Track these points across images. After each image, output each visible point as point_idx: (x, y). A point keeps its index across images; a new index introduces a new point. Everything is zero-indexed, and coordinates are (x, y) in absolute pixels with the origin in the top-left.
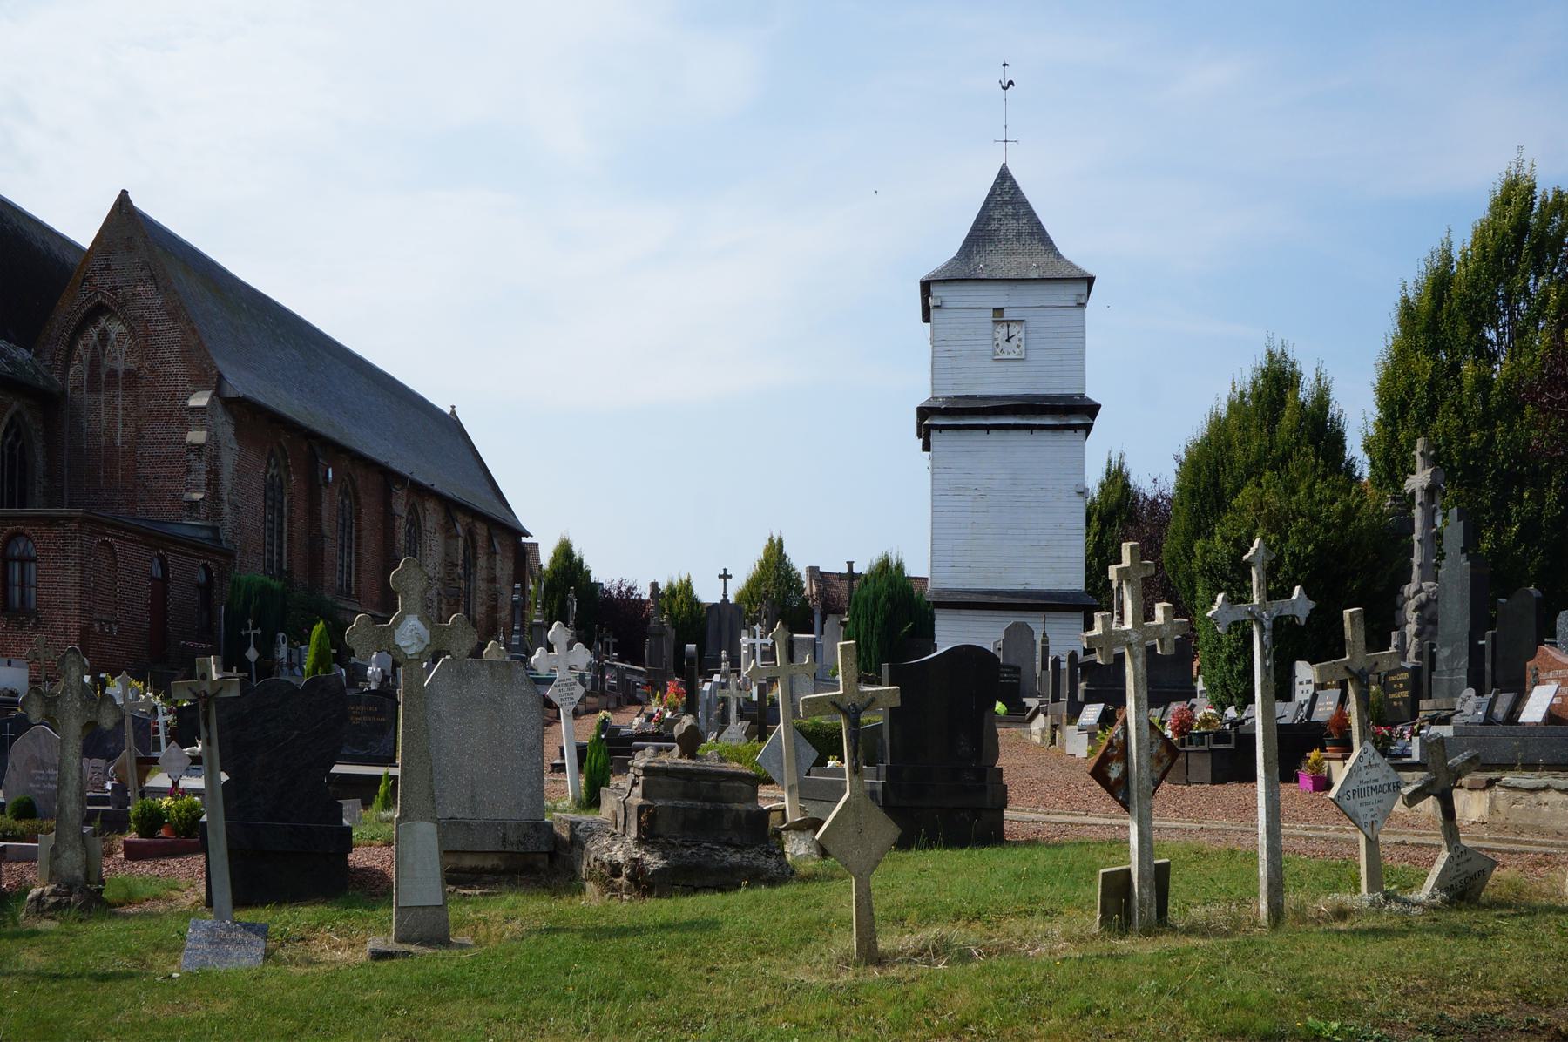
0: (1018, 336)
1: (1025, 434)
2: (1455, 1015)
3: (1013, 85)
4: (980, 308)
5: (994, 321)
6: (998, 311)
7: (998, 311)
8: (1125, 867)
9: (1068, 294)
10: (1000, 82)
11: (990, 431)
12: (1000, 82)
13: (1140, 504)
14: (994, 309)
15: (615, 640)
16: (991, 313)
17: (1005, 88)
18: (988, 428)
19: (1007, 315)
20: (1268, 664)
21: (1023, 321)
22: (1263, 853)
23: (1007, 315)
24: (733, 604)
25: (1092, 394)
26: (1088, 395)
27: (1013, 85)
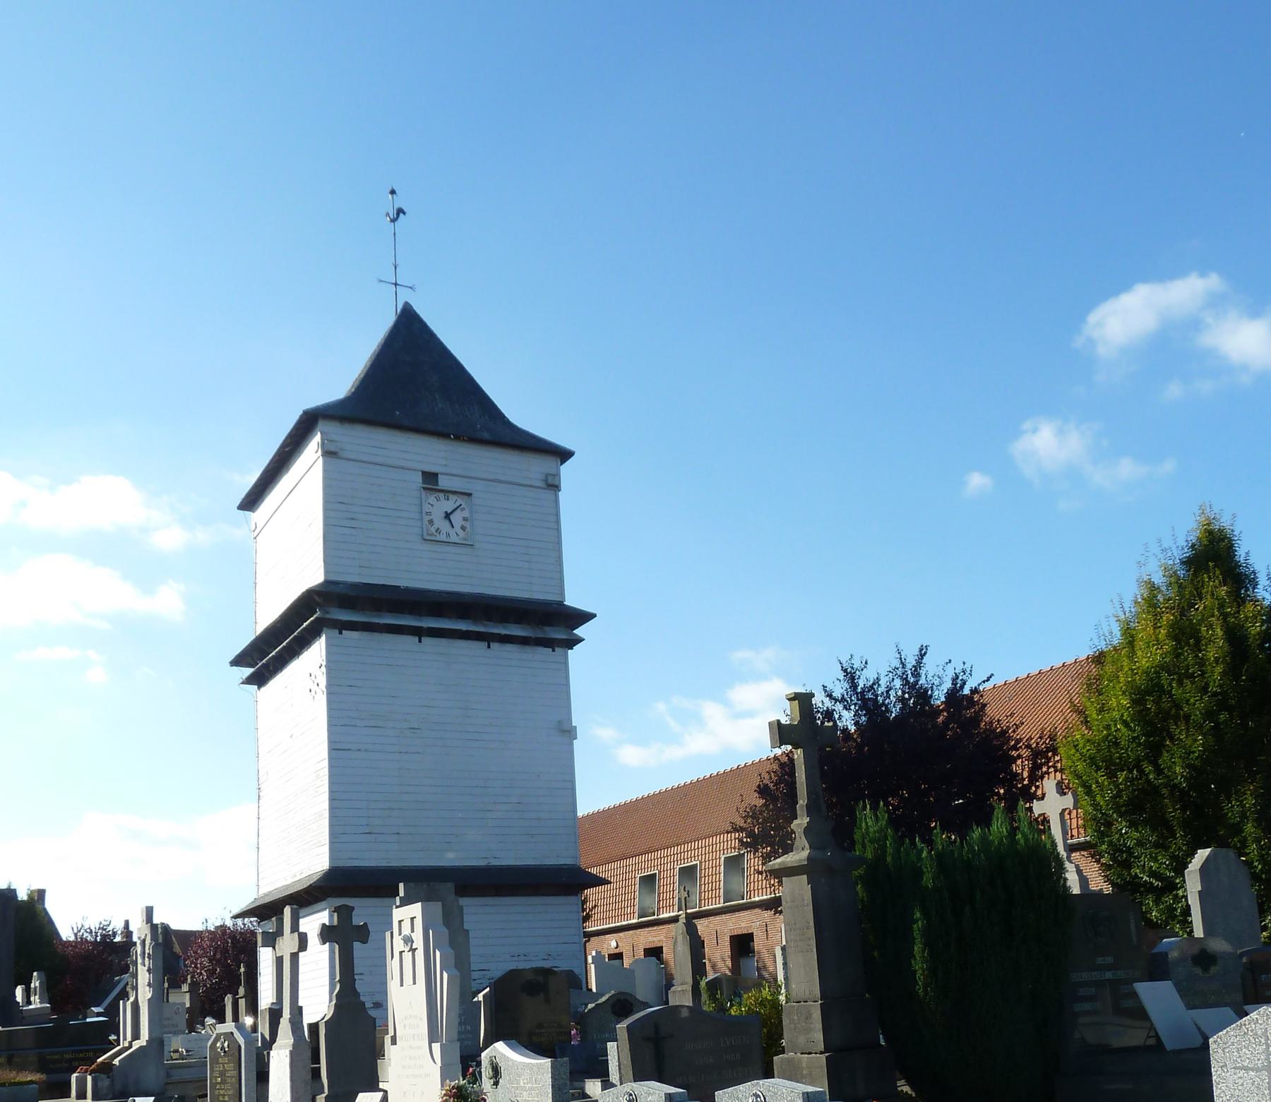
0: (452, 532)
1: (477, 647)
2: (235, 1035)
3: (404, 213)
4: (402, 468)
5: (423, 488)
6: (430, 478)
7: (430, 478)
8: (775, 1072)
9: (535, 466)
11: (423, 639)
13: (237, 997)
14: (424, 473)
15: (448, 1081)
16: (418, 478)
17: (393, 221)
18: (419, 633)
20: (934, 824)
21: (469, 495)
22: (263, 1028)
23: (443, 482)
24: (22, 901)
25: (574, 599)
26: (569, 602)
27: (404, 213)
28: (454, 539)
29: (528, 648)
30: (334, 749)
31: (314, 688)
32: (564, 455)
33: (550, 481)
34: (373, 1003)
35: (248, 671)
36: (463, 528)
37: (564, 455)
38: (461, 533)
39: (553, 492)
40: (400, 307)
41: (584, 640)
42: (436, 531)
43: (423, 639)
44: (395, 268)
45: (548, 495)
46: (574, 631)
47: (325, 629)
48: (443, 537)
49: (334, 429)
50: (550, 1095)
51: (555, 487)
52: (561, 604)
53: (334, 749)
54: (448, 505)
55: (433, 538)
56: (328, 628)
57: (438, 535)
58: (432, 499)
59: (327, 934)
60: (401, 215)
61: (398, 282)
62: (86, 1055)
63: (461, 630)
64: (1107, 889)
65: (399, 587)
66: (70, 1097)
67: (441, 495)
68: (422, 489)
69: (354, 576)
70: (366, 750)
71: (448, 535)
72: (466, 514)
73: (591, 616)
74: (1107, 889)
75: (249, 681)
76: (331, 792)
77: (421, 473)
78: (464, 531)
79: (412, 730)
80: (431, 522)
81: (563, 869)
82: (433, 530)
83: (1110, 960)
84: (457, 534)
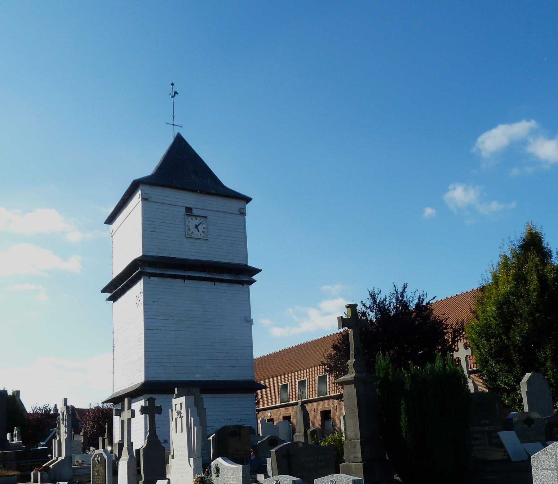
1: (209, 284)
6: (189, 210)
7: (189, 210)
9: (235, 205)
16: (184, 210)
21: (206, 217)
23: (195, 212)
25: (252, 263)
28: (199, 237)
29: (232, 285)
30: (147, 329)
31: (138, 302)
32: (248, 200)
33: (242, 211)
35: (109, 295)
36: (203, 232)
37: (248, 200)
38: (203, 234)
39: (243, 216)
41: (256, 281)
42: (192, 233)
44: (174, 118)
45: (240, 217)
46: (252, 277)
47: (143, 276)
48: (194, 236)
49: (147, 188)
50: (242, 481)
51: (244, 214)
53: (147, 329)
54: (197, 222)
55: (190, 236)
56: (144, 276)
57: (192, 235)
58: (190, 219)
61: (175, 124)
63: (202, 277)
64: (486, 390)
65: (175, 258)
67: (194, 218)
68: (185, 215)
69: (155, 253)
70: (161, 330)
71: (197, 235)
72: (205, 226)
74: (486, 390)
75: (109, 299)
76: (145, 348)
77: (185, 208)
78: (204, 233)
79: (181, 321)
80: (189, 229)
82: (190, 233)
84: (200, 234)
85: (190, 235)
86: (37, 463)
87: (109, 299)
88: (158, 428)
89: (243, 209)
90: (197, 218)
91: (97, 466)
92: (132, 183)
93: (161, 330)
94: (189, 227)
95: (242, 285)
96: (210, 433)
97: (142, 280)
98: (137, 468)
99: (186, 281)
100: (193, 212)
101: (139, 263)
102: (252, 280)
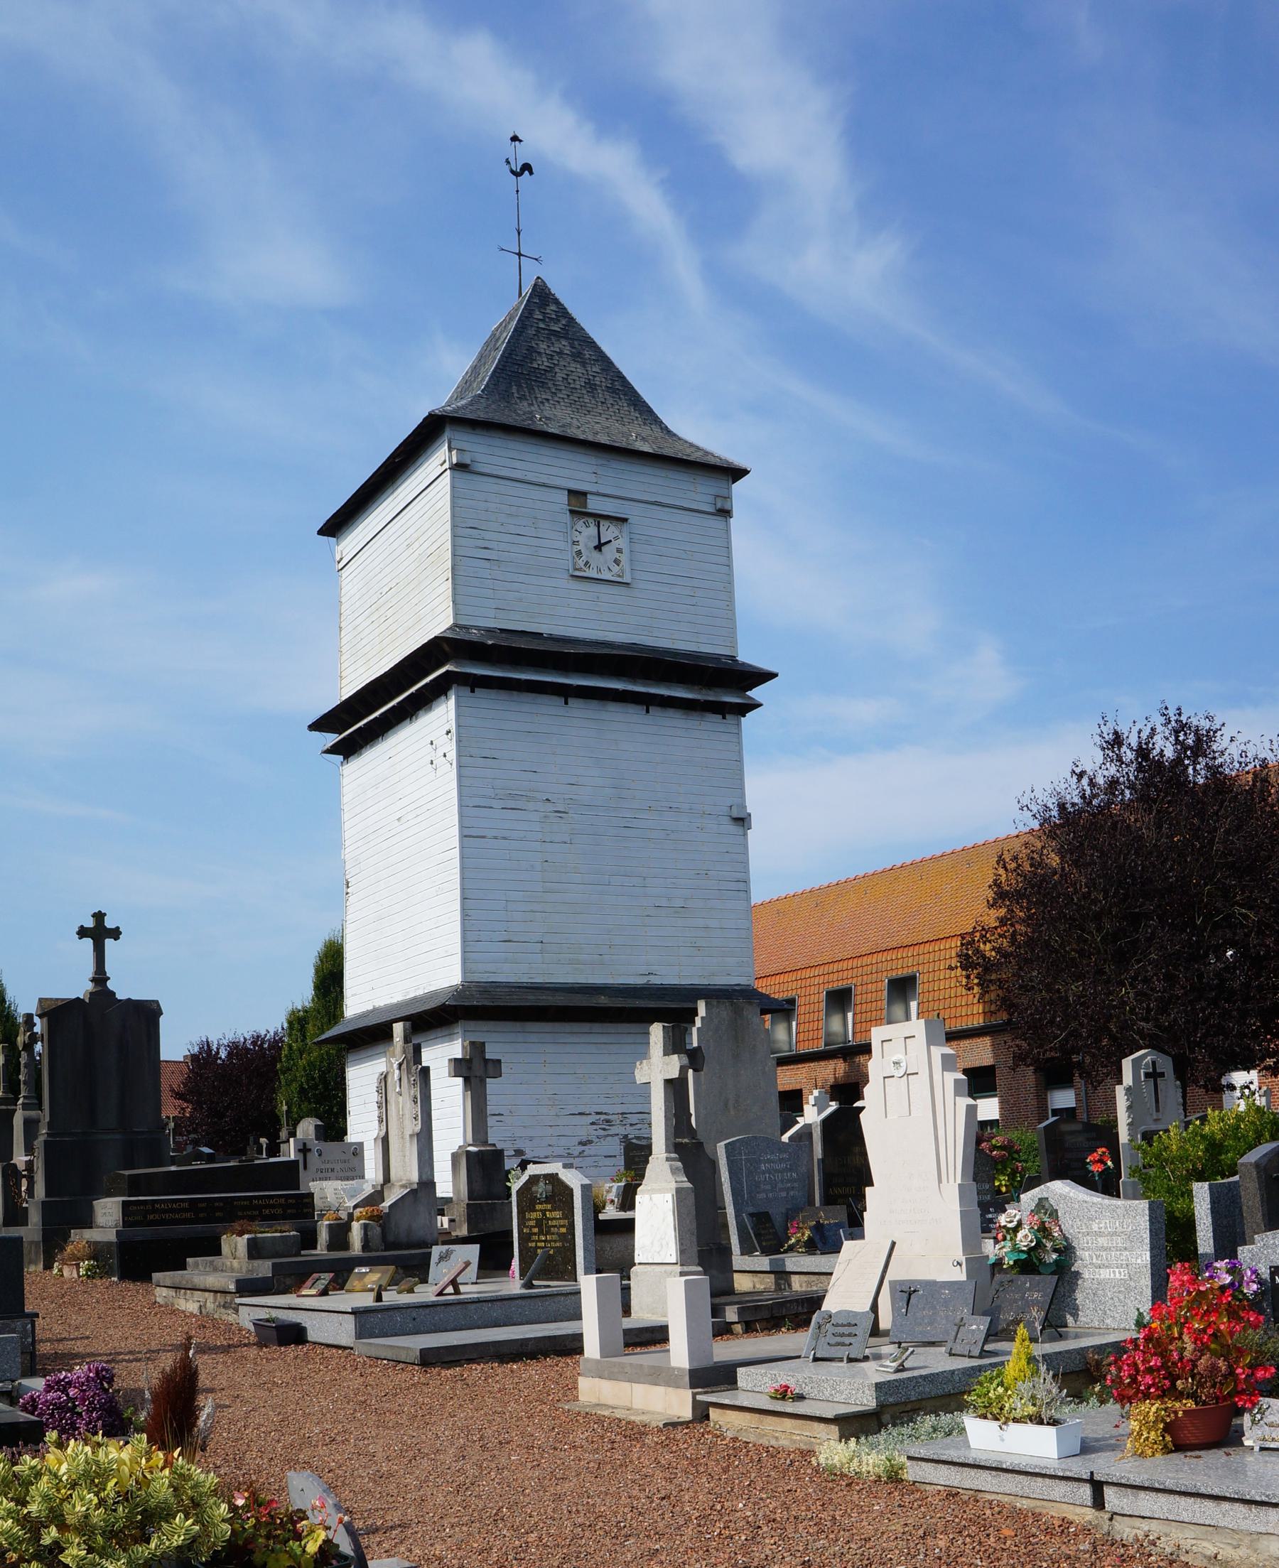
3: (531, 173)
6: (577, 495)
7: (577, 495)
9: (699, 492)
10: (508, 162)
12: (508, 162)
16: (563, 498)
19: (594, 505)
25: (749, 655)
27: (531, 173)
29: (695, 715)
30: (466, 836)
31: (440, 761)
32: (738, 473)
34: (515, 1151)
35: (332, 739)
37: (738, 473)
40: (527, 289)
41: (760, 705)
42: (585, 565)
43: (570, 700)
44: (519, 234)
45: (717, 522)
46: (747, 693)
47: (454, 686)
48: (592, 573)
50: (1148, 1241)
51: (725, 513)
52: (733, 658)
56: (458, 685)
58: (580, 524)
59: (460, 1067)
60: (527, 172)
61: (522, 253)
62: (180, 1205)
63: (617, 690)
65: (542, 634)
66: (221, 1255)
70: (505, 838)
73: (772, 676)
75: (333, 750)
77: (566, 492)
78: (618, 565)
80: (579, 553)
81: (735, 990)
82: (581, 563)
83: (217, 1204)
85: (580, 570)
86: (276, 1201)
87: (333, 750)
88: (499, 1114)
89: (725, 498)
90: (599, 523)
91: (537, 1208)
92: (425, 419)
93: (505, 838)
94: (579, 548)
95: (721, 716)
96: (637, 1132)
97: (452, 702)
98: (817, 1204)
99: (570, 700)
100: (589, 506)
101: (446, 648)
102: (750, 702)
